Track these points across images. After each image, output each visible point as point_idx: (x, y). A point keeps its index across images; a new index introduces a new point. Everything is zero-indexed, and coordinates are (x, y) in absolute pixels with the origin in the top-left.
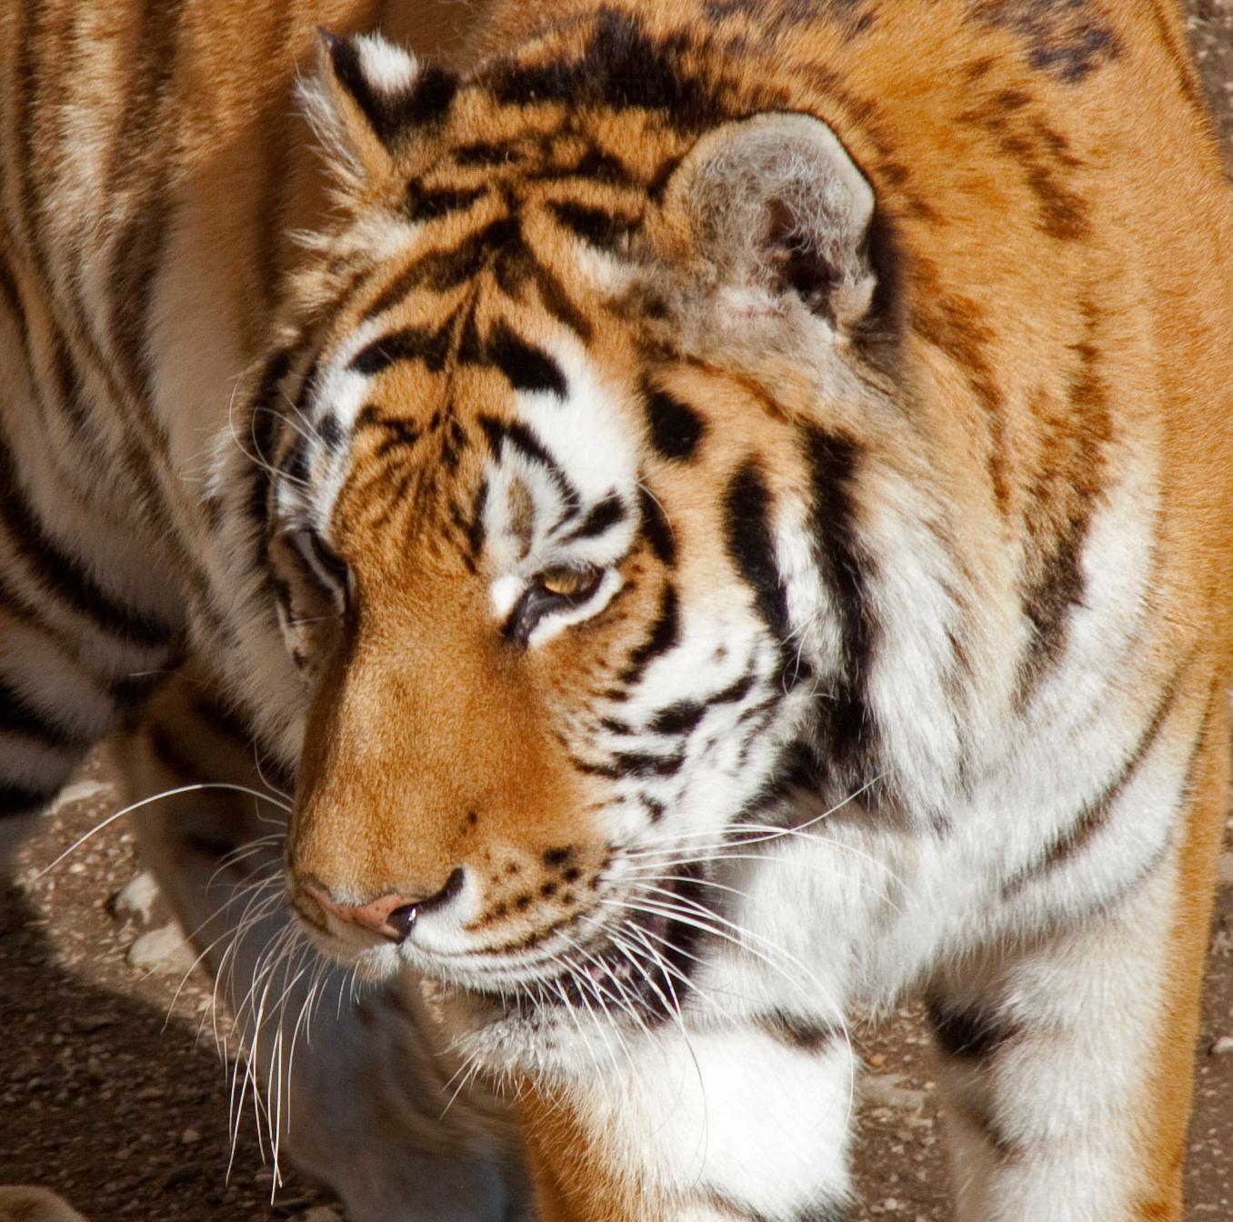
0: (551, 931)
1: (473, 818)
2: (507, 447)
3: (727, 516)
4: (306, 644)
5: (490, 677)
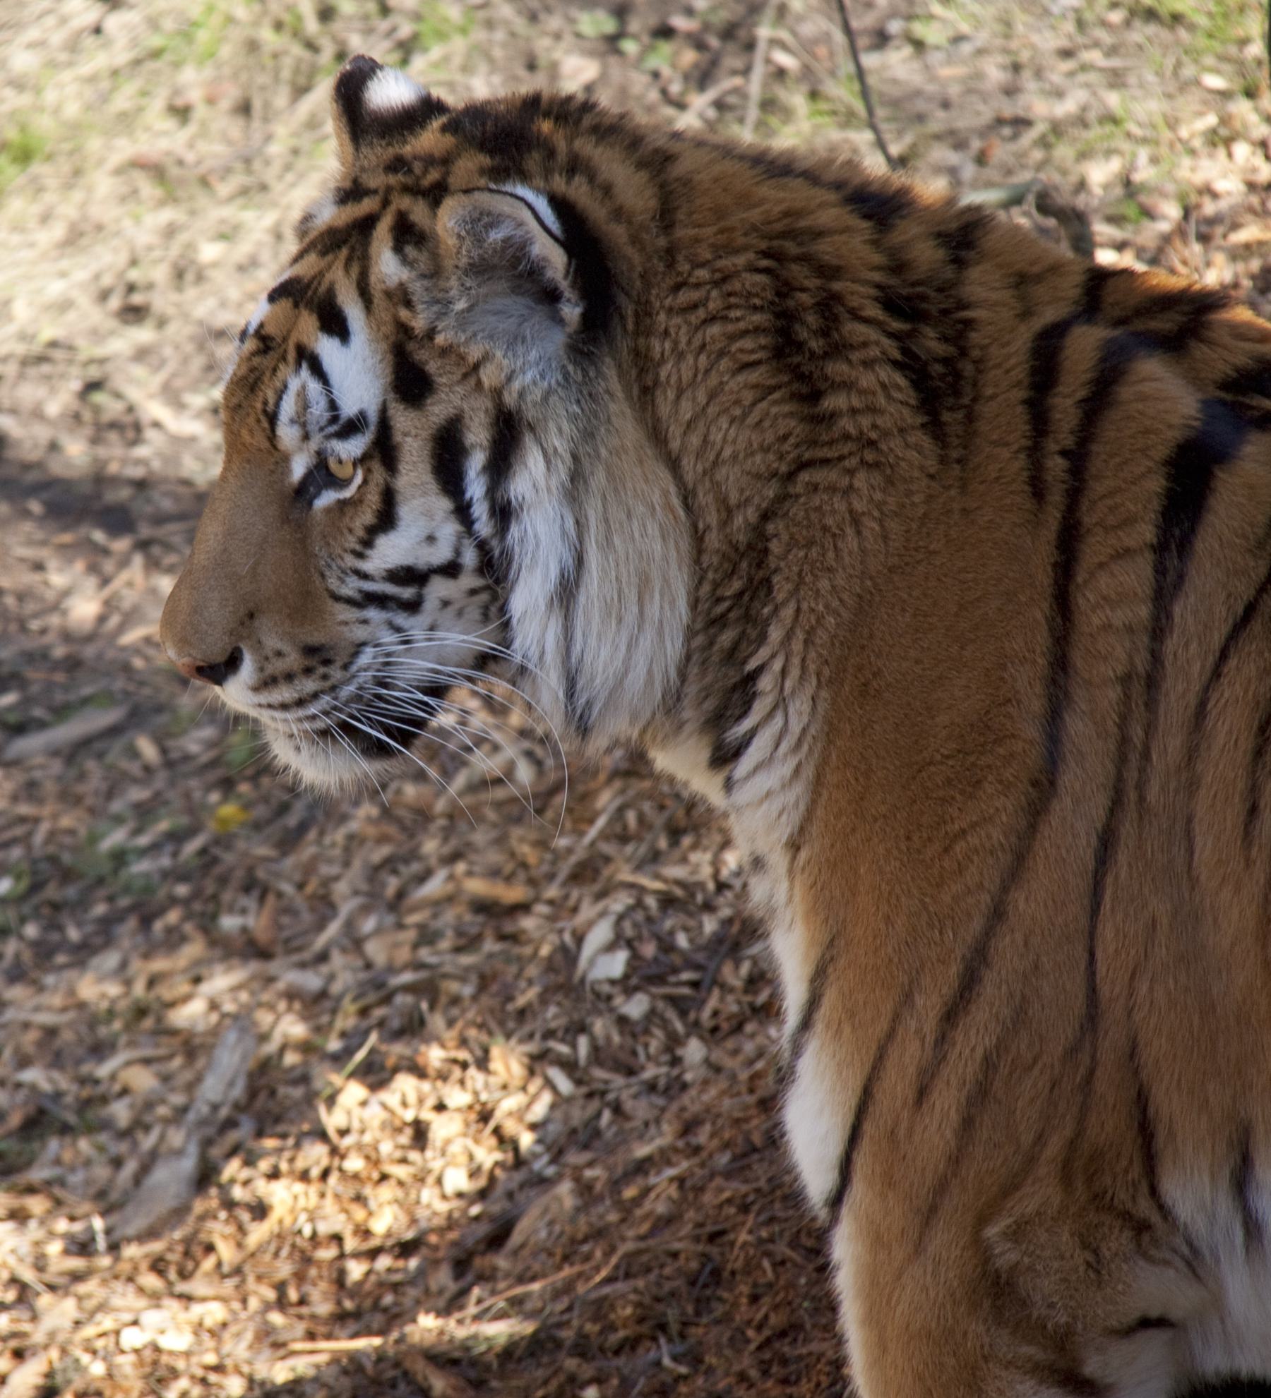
0: (315, 696)
1: (251, 616)
2: (304, 365)
3: (434, 448)
5: (283, 523)
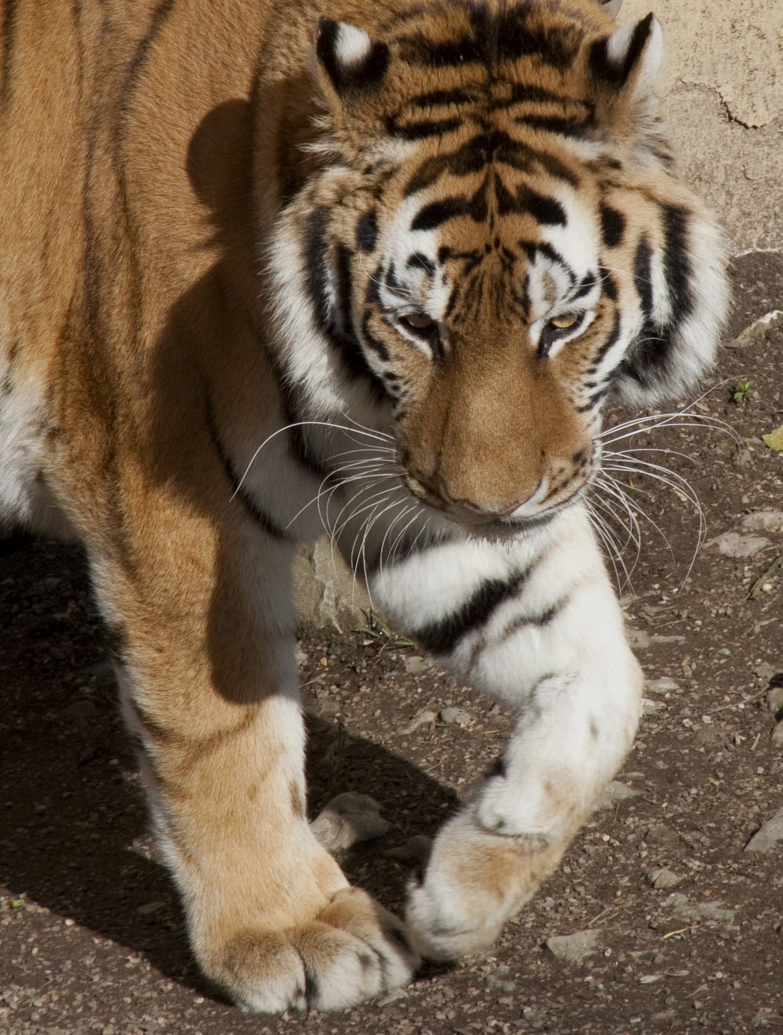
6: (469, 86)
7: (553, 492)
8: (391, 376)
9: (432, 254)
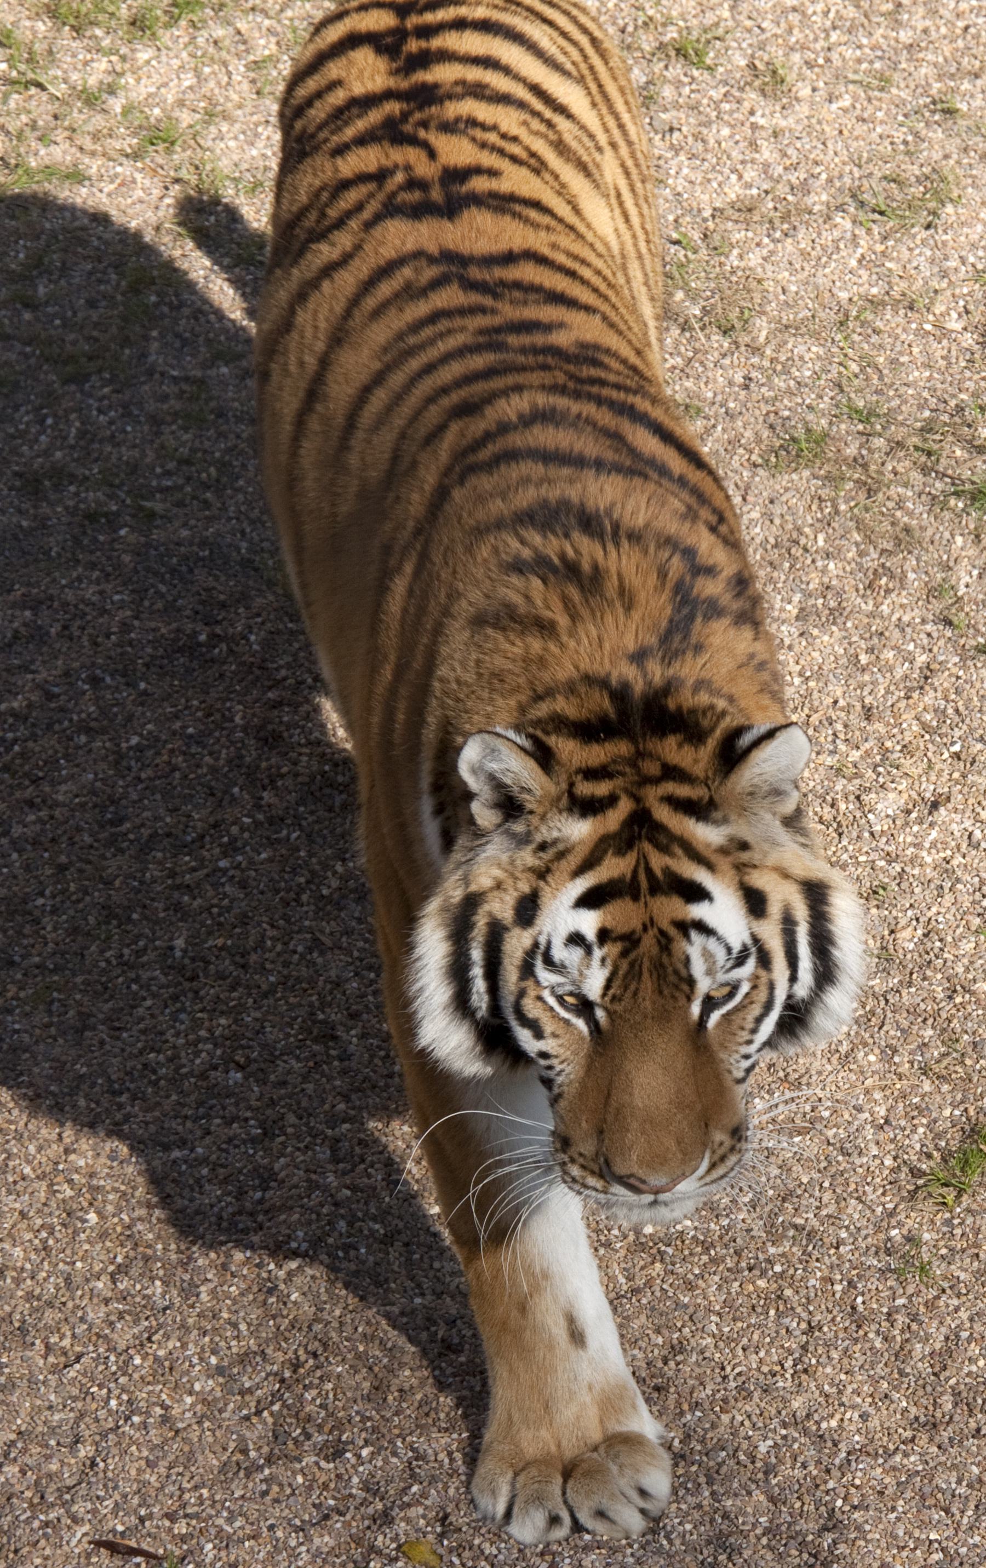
2: (694, 935)
4: (487, 1061)
6: (614, 761)
7: (713, 1166)
8: (544, 1055)
9: (590, 934)
